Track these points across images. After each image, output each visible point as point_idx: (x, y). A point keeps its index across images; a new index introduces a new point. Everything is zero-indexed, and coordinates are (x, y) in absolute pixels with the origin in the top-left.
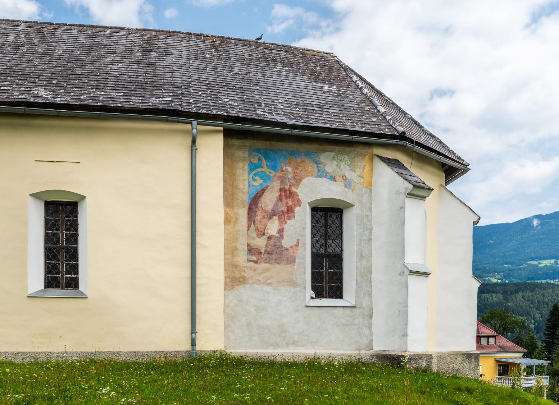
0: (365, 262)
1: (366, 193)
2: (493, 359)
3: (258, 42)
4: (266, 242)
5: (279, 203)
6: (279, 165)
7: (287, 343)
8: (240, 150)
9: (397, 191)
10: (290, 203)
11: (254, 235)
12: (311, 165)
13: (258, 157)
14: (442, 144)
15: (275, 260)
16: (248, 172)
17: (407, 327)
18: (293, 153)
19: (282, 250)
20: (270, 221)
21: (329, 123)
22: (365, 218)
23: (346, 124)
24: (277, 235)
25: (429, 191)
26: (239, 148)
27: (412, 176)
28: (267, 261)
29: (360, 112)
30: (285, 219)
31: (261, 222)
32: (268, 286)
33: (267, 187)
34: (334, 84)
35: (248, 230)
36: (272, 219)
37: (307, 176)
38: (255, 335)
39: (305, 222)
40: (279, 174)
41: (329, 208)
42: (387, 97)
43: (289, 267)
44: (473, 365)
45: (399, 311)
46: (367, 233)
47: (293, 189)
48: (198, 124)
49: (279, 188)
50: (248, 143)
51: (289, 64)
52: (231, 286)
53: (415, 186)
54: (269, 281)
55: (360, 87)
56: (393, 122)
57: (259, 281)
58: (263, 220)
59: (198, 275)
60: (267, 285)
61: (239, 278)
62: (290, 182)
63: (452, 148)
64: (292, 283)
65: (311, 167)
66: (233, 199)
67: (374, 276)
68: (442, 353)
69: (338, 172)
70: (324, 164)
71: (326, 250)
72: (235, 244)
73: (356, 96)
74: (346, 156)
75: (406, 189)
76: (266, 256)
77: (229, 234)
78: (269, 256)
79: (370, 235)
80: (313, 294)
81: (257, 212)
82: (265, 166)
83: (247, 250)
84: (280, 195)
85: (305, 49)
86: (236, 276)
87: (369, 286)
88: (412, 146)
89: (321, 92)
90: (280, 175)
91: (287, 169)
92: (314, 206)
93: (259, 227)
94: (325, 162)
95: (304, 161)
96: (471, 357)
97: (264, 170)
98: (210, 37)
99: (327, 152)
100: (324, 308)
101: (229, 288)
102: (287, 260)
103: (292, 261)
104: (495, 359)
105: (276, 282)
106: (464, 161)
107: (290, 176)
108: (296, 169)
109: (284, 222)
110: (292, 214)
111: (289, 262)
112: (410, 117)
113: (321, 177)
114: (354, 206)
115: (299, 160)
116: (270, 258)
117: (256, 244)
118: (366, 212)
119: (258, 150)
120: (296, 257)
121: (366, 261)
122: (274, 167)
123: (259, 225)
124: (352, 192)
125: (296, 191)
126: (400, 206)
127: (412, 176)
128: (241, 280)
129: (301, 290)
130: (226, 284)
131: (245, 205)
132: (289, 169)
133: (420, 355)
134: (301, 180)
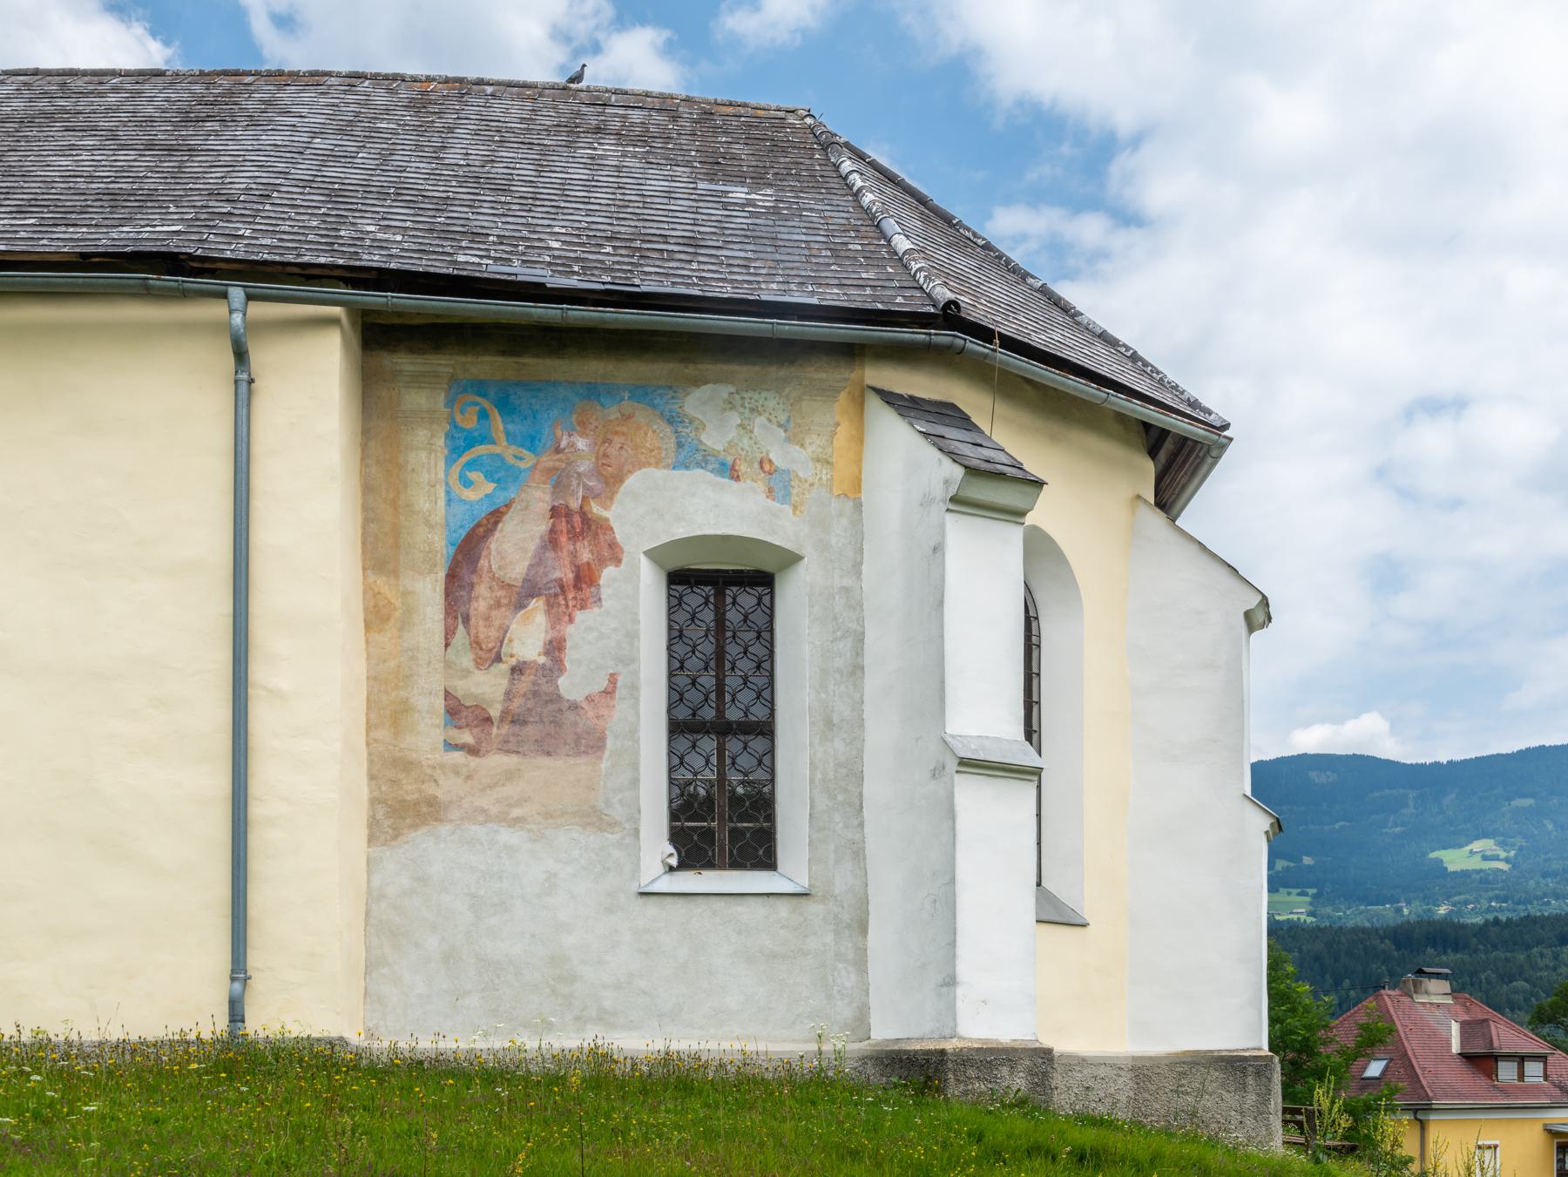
0: (839, 745)
1: (840, 515)
2: (1539, 1128)
3: (570, 89)
4: (505, 682)
5: (547, 555)
6: (546, 431)
7: (578, 1019)
8: (420, 388)
9: (925, 495)
10: (585, 556)
11: (467, 660)
12: (655, 427)
13: (477, 408)
14: (1140, 363)
15: (536, 741)
16: (446, 458)
17: (954, 955)
18: (593, 392)
19: (560, 710)
20: (518, 615)
21: (699, 285)
22: (837, 597)
23: (763, 286)
24: (542, 660)
25: (1029, 489)
26: (417, 380)
27: (981, 446)
28: (511, 746)
29: (829, 254)
30: (567, 606)
31: (487, 619)
32: (512, 830)
33: (508, 506)
34: (770, 185)
35: (447, 645)
36: (525, 607)
37: (642, 465)
38: (470, 992)
39: (636, 614)
40: (548, 460)
41: (727, 571)
42: (969, 230)
43: (582, 765)
44: (1251, 1098)
45: (935, 901)
46: (845, 646)
47: (596, 509)
48: (250, 298)
49: (549, 508)
50: (446, 365)
51: (644, 138)
52: (390, 831)
53: (972, 471)
54: (516, 812)
55: (855, 189)
56: (925, 277)
57: (484, 811)
58: (494, 613)
59: (256, 788)
60: (509, 826)
61: (416, 804)
62: (585, 485)
63: (1172, 376)
64: (595, 819)
65: (655, 435)
66: (396, 546)
67: (868, 789)
68: (1150, 1058)
69: (747, 448)
70: (697, 422)
71: (720, 711)
72: (403, 694)
73: (832, 214)
74: (770, 395)
75: (947, 482)
76: (506, 729)
77: (385, 661)
78: (516, 729)
79: (857, 654)
80: (671, 855)
81: (477, 588)
82: (502, 436)
83: (442, 711)
84: (552, 531)
85: (719, 101)
86: (408, 798)
87: (856, 823)
88: (987, 351)
89: (715, 205)
90: (551, 464)
91: (572, 445)
92: (677, 563)
93: (482, 636)
94: (700, 417)
95: (630, 417)
96: (1244, 1070)
97: (497, 449)
98: (421, 81)
99: (706, 383)
100: (700, 900)
101: (383, 838)
102: (577, 742)
103: (591, 743)
104: (1545, 1125)
105: (539, 814)
106: (1210, 413)
107: (584, 466)
108: (604, 442)
109: (567, 618)
110: (593, 589)
111: (583, 748)
112: (1040, 284)
113: (687, 468)
114: (803, 558)
115: (613, 414)
116: (518, 735)
117: (473, 690)
118: (841, 577)
119: (480, 387)
120: (607, 732)
121: (844, 739)
122: (533, 439)
123: (481, 629)
124: (794, 513)
125: (606, 514)
126: (933, 544)
127: (981, 446)
128: (424, 809)
129: (623, 839)
130: (373, 823)
131: (435, 566)
132: (581, 443)
133: (1005, 1050)
134: (619, 479)
